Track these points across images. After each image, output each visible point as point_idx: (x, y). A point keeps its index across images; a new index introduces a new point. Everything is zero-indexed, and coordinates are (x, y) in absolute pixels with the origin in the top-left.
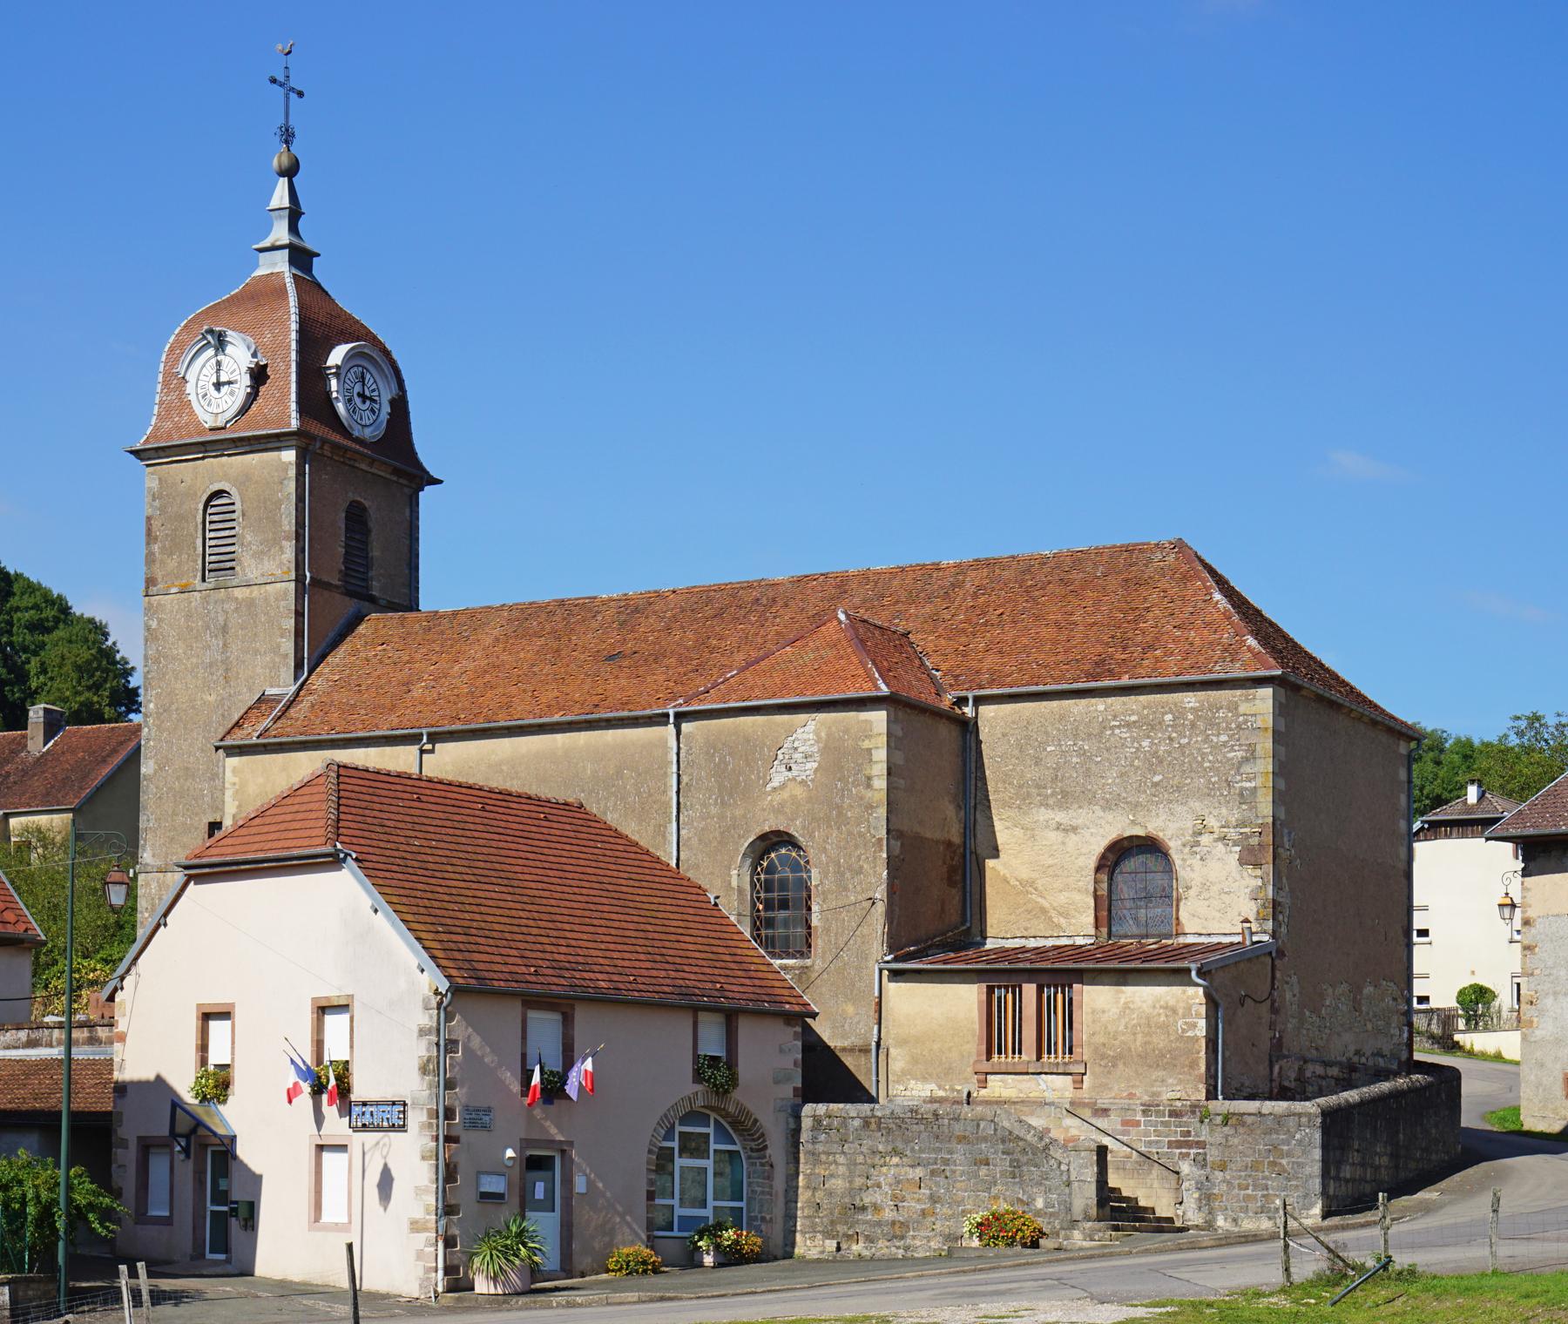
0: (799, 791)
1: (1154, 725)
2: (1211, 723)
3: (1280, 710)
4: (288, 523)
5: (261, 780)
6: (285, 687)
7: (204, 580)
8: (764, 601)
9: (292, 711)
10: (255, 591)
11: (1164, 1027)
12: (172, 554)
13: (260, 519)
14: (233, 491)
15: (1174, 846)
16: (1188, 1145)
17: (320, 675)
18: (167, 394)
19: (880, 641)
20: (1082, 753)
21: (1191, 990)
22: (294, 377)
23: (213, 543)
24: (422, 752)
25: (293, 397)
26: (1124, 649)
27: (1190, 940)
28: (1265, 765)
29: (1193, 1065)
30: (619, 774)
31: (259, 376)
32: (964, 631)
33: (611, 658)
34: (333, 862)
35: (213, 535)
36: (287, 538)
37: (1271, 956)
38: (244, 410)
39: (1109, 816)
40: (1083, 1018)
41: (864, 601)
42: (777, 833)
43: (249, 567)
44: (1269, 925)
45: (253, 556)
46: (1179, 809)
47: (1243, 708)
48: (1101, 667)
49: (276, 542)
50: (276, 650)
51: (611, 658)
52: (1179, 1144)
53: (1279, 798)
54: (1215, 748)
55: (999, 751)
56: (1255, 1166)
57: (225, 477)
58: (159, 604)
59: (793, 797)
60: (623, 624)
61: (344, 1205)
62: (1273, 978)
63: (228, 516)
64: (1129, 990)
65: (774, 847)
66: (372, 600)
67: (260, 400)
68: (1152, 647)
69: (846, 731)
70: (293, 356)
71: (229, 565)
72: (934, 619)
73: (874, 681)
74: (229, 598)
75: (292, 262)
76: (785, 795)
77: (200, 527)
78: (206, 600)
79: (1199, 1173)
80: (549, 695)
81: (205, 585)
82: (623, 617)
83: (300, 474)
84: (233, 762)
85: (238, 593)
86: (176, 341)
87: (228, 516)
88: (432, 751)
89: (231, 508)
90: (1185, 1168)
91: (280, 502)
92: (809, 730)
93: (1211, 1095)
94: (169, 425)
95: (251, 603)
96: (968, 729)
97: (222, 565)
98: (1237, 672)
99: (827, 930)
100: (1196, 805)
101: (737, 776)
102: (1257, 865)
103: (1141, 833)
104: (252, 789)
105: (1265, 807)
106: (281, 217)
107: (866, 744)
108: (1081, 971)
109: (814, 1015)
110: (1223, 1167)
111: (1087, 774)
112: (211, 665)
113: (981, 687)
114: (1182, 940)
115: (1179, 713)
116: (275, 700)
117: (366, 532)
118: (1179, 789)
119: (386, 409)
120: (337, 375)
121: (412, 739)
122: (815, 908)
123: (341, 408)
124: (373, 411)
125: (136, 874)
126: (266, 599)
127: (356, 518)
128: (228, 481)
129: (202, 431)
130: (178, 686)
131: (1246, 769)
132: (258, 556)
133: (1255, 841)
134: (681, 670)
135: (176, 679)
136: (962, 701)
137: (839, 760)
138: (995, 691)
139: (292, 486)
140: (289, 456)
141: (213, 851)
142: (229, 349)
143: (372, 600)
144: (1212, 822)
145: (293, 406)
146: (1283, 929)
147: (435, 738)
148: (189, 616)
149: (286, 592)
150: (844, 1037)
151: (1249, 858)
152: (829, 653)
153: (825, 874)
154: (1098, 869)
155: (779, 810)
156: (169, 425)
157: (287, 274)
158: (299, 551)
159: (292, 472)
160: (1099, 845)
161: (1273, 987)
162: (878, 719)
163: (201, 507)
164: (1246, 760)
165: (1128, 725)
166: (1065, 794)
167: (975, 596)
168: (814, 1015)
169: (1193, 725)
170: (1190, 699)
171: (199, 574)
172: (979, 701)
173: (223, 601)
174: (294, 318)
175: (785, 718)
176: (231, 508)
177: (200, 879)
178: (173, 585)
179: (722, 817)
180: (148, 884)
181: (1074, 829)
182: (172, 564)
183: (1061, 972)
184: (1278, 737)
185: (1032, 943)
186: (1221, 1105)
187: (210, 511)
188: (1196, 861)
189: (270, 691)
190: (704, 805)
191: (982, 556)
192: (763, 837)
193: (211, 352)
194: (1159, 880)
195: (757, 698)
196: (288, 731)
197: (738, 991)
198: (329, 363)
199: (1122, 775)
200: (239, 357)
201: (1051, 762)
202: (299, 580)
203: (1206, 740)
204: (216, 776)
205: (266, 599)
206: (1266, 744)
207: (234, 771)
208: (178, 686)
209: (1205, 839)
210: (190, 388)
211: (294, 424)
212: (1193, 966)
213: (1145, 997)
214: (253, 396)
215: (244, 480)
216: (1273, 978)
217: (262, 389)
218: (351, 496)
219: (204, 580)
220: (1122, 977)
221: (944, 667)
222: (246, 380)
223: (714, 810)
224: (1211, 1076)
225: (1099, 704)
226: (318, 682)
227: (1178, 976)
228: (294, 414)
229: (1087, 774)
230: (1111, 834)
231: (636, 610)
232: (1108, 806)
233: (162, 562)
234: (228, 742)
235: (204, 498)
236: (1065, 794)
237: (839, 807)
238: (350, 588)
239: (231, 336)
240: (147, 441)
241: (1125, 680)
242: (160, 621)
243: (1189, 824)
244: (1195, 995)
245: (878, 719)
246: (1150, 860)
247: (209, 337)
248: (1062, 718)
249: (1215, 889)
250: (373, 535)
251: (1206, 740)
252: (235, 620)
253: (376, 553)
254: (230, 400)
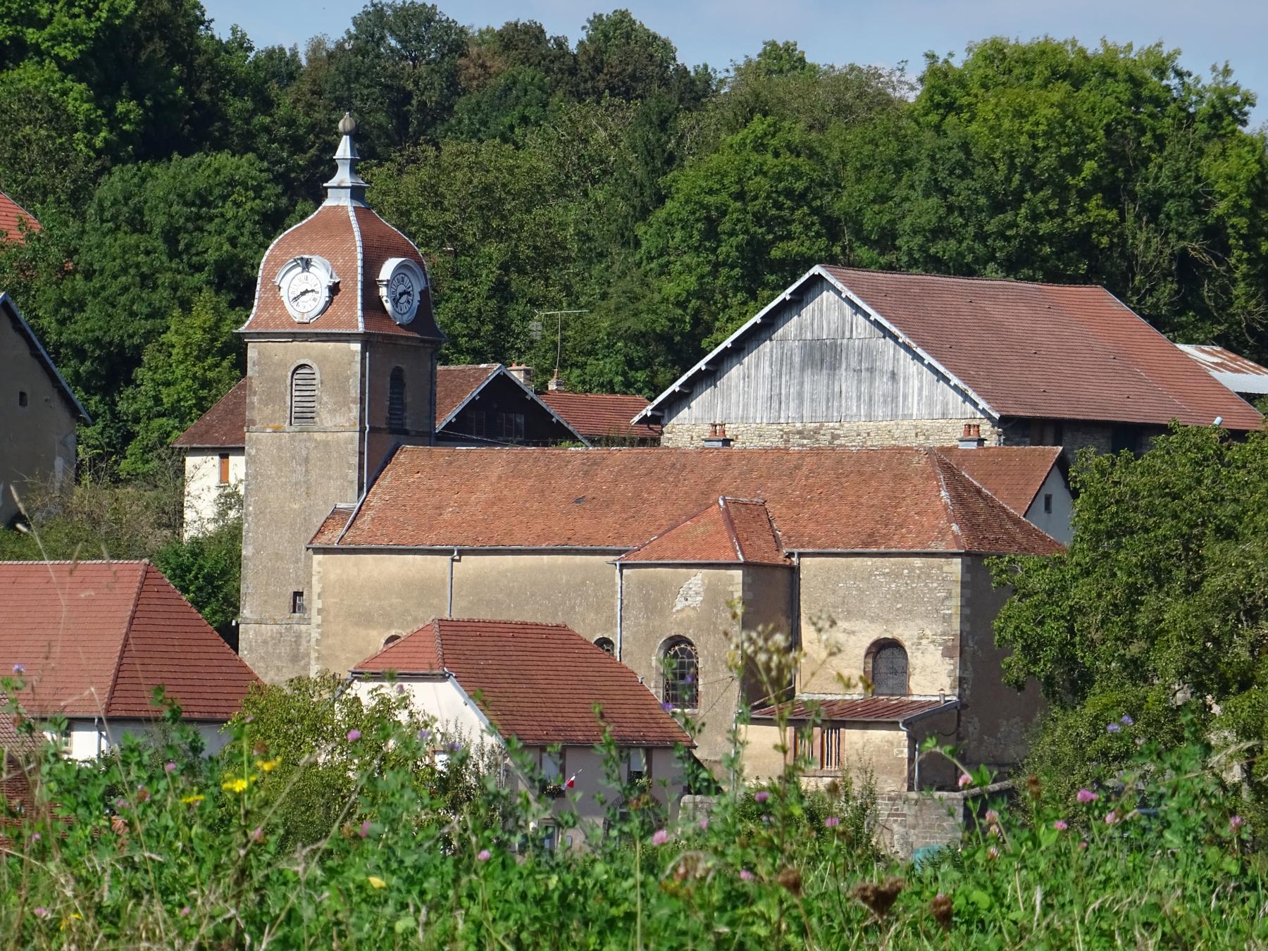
0: (692, 614)
1: (898, 575)
2: (929, 576)
3: (966, 569)
4: (355, 392)
5: (339, 571)
6: (350, 502)
8: (678, 466)
9: (358, 522)
10: (330, 437)
11: (887, 752)
12: (267, 405)
14: (314, 366)
15: (907, 645)
16: (898, 815)
17: (374, 494)
18: (265, 293)
19: (745, 518)
20: (859, 589)
21: (901, 733)
22: (359, 293)
24: (453, 560)
25: (359, 306)
26: (886, 526)
27: (915, 698)
28: (956, 602)
29: (901, 773)
30: (583, 583)
31: (334, 289)
32: (798, 503)
33: (578, 501)
34: (444, 678)
36: (354, 402)
37: (960, 707)
38: (323, 311)
39: (873, 626)
40: (846, 745)
41: (740, 474)
42: (679, 636)
43: (326, 419)
44: (957, 691)
45: (329, 412)
46: (911, 623)
47: (946, 569)
48: (871, 539)
49: (345, 404)
50: (345, 477)
51: (578, 501)
52: (894, 815)
53: (964, 619)
54: (931, 590)
55: (813, 584)
56: (931, 826)
57: (309, 356)
59: (689, 617)
60: (586, 473)
61: (1080, 949)
62: (959, 720)
64: (869, 732)
65: (677, 644)
66: (406, 433)
67: (334, 305)
68: (901, 526)
69: (719, 580)
70: (359, 277)
71: (310, 415)
72: (781, 492)
73: (736, 551)
74: (310, 439)
75: (353, 197)
76: (684, 615)
78: (293, 439)
79: (902, 830)
80: (538, 527)
81: (293, 428)
82: (586, 468)
83: (363, 358)
84: (318, 558)
85: (317, 436)
88: (459, 561)
90: (895, 827)
91: (347, 379)
92: (698, 578)
93: (910, 789)
94: (266, 315)
95: (326, 444)
96: (794, 571)
98: (941, 549)
99: (707, 693)
100: (919, 622)
101: (655, 602)
102: (951, 658)
103: (890, 637)
104: (332, 577)
105: (956, 625)
107: (730, 589)
108: (844, 722)
109: (695, 747)
110: (914, 828)
111: (861, 601)
112: (296, 484)
113: (803, 547)
114: (911, 698)
115: (912, 569)
116: (346, 513)
117: (403, 385)
118: (910, 612)
119: (417, 298)
120: (387, 286)
121: (450, 552)
122: (700, 681)
123: (388, 306)
125: (238, 625)
127: (397, 378)
129: (292, 324)
130: (271, 496)
131: (947, 603)
132: (333, 412)
133: (950, 644)
134: (625, 516)
135: (270, 491)
136: (791, 555)
137: (713, 594)
138: (810, 550)
140: (356, 347)
141: (371, 665)
142: (312, 269)
143: (406, 433)
144: (928, 632)
145: (360, 313)
146: (968, 692)
147: (461, 553)
148: (280, 449)
150: (716, 755)
151: (947, 653)
152: (711, 528)
153: (706, 662)
154: (866, 656)
155: (680, 623)
157: (350, 209)
158: (362, 410)
159: (358, 358)
160: (867, 642)
161: (958, 725)
162: (738, 574)
164: (946, 598)
165: (884, 574)
166: (849, 612)
167: (807, 478)
168: (695, 747)
169: (919, 577)
170: (918, 562)
172: (801, 555)
174: (359, 250)
175: (684, 570)
177: (360, 680)
178: (268, 426)
179: (647, 625)
180: (246, 632)
181: (853, 633)
182: (268, 411)
183: (838, 719)
184: (964, 585)
185: (829, 698)
186: (914, 795)
188: (919, 654)
189: (341, 505)
190: (636, 618)
191: (1022, 33)
192: (671, 638)
194: (901, 661)
195: (668, 558)
196: (359, 536)
197: (653, 735)
198: (381, 278)
199: (880, 603)
201: (841, 593)
202: (362, 431)
203: (926, 585)
204: (308, 566)
206: (957, 590)
207: (319, 563)
208: (271, 496)
209: (924, 642)
211: (361, 328)
212: (901, 720)
213: (878, 736)
214: (330, 302)
215: (323, 359)
216: (959, 720)
218: (394, 364)
220: (866, 725)
221: (784, 529)
222: (326, 293)
223: (642, 622)
224: (911, 778)
225: (869, 561)
226: (374, 501)
227: (893, 726)
228: (360, 319)
229: (861, 601)
230: (874, 637)
231: (595, 463)
232: (872, 620)
234: (316, 544)
236: (849, 612)
237: (715, 624)
239: (316, 260)
241: (882, 549)
242: (258, 450)
243: (916, 633)
244: (902, 735)
245: (738, 574)
246: (896, 651)
248: (848, 568)
249: (929, 670)
251: (926, 585)
252: (314, 455)
253: (408, 399)
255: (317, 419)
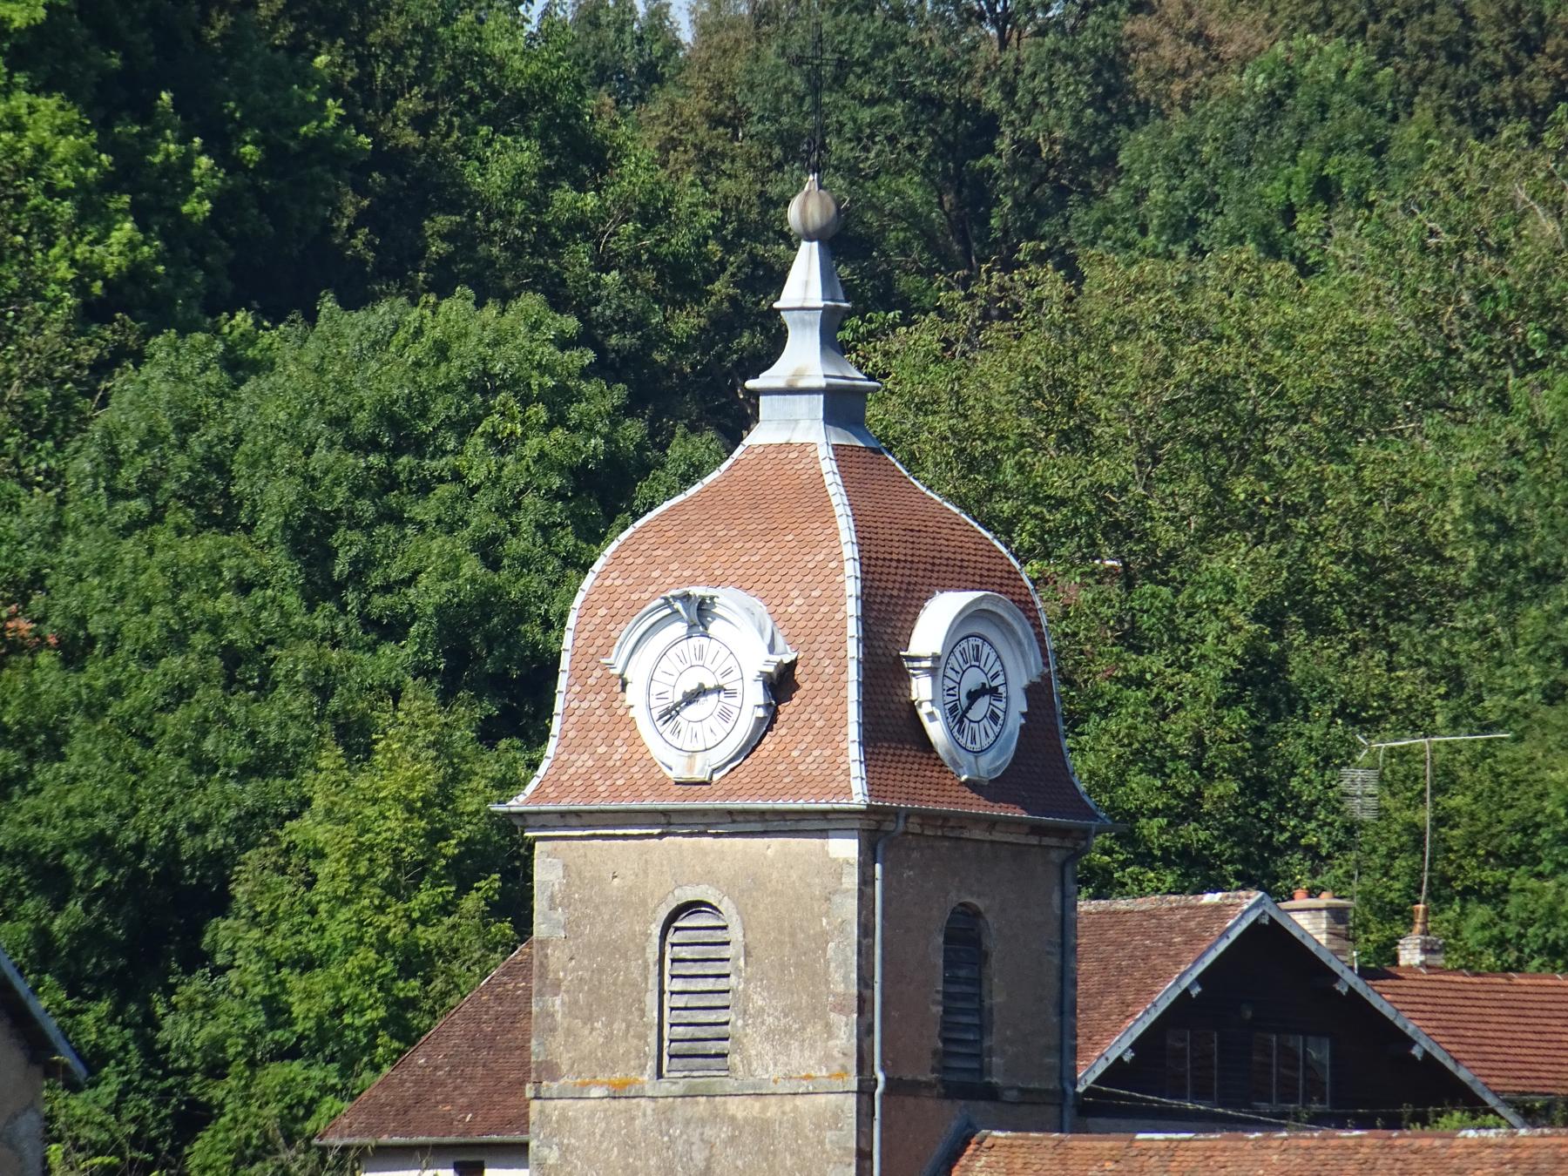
4: (843, 981)
7: (660, 1075)
10: (773, 1108)
13: (783, 967)
14: (726, 906)
22: (853, 693)
23: (680, 1001)
25: (853, 731)
31: (780, 684)
35: (678, 985)
36: (840, 1008)
38: (750, 747)
43: (760, 1057)
57: (710, 877)
58: (564, 1117)
63: (717, 1001)
67: (780, 730)
74: (715, 1117)
77: (654, 970)
78: (665, 1117)
81: (664, 1086)
83: (866, 881)
85: (735, 1107)
86: (597, 589)
87: (717, 1001)
89: (719, 936)
91: (823, 938)
94: (584, 761)
95: (763, 1129)
97: (699, 1047)
106: (804, 324)
117: (979, 957)
119: (1019, 705)
120: (932, 672)
123: (937, 731)
124: (994, 717)
126: (795, 1125)
127: (964, 937)
128: (714, 883)
129: (661, 786)
132: (780, 1037)
139: (852, 905)
142: (715, 628)
143: (991, 1094)
148: (628, 1145)
149: (837, 1116)
156: (584, 761)
158: (865, 1032)
159: (851, 881)
163: (656, 930)
171: (652, 1064)
173: (703, 1122)
176: (719, 936)
182: (592, 1038)
187: (672, 937)
193: (679, 628)
198: (914, 650)
200: (743, 644)
202: (865, 1091)
205: (795, 1125)
210: (634, 695)
211: (858, 795)
217: (786, 709)
218: (954, 898)
219: (660, 1075)
222: (756, 695)
228: (857, 770)
233: (569, 1032)
235: (663, 913)
238: (954, 1078)
239: (728, 600)
240: (527, 803)
242: (565, 1151)
247: (678, 605)
250: (994, 961)
253: (997, 997)
254: (721, 728)
255: (734, 1059)
